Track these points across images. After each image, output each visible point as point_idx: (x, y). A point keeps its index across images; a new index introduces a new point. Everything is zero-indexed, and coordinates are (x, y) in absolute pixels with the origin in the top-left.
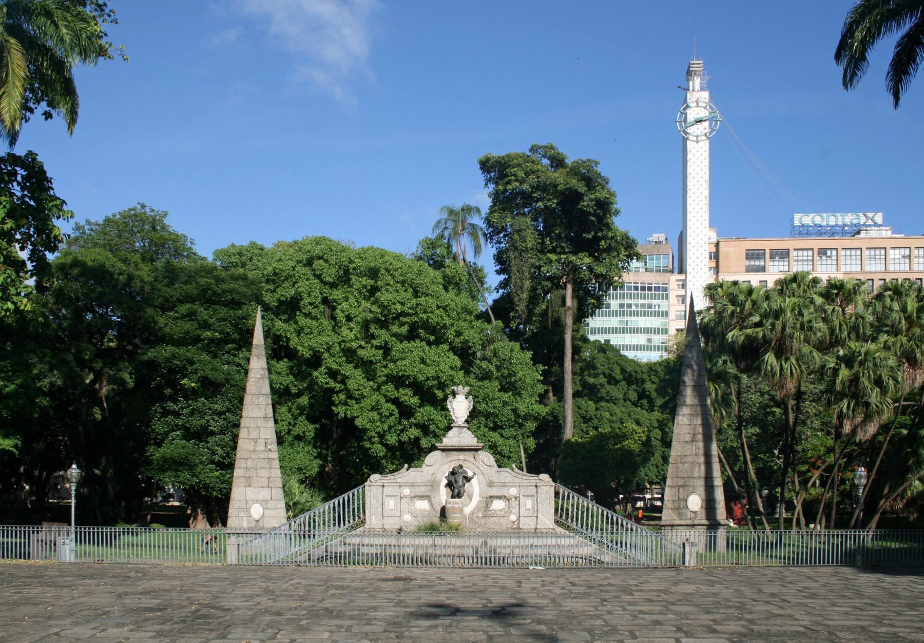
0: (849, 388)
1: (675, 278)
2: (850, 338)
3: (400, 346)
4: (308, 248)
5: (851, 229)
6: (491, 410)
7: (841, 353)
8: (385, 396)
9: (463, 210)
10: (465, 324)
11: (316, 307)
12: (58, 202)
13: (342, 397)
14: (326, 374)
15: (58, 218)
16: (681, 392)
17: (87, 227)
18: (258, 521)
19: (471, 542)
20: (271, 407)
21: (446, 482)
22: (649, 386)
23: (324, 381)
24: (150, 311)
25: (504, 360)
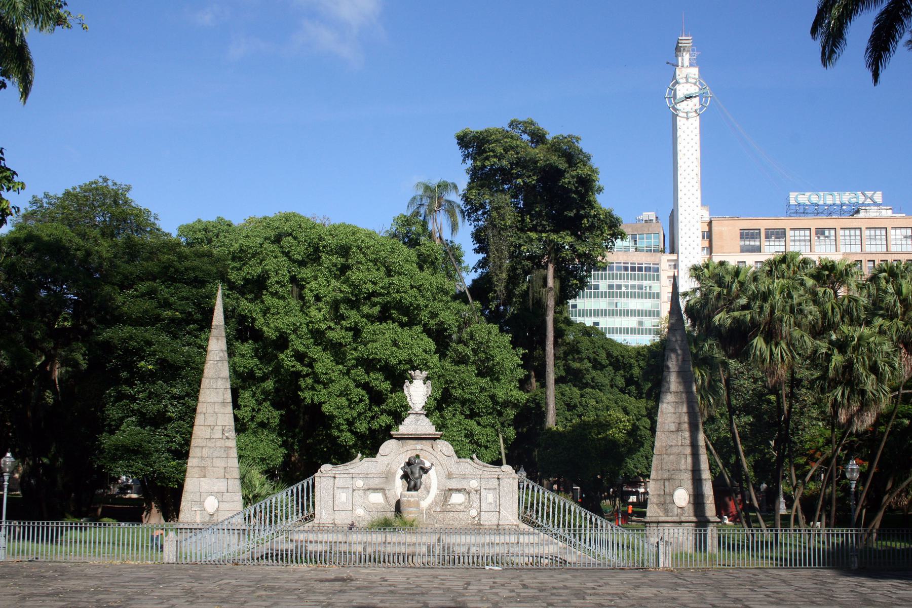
0: (843, 374)
1: (666, 258)
2: (843, 321)
3: (370, 328)
4: (277, 224)
5: (850, 208)
6: (468, 396)
7: (834, 337)
8: (355, 381)
9: (439, 186)
10: (440, 305)
11: (284, 286)
12: (8, 173)
13: (309, 381)
14: (292, 356)
15: (8, 190)
16: (666, 377)
17: (45, 200)
18: (212, 515)
19: (424, 539)
20: (229, 391)
21: (402, 473)
22: (636, 371)
23: (289, 363)
24: (108, 288)
25: (481, 343)
